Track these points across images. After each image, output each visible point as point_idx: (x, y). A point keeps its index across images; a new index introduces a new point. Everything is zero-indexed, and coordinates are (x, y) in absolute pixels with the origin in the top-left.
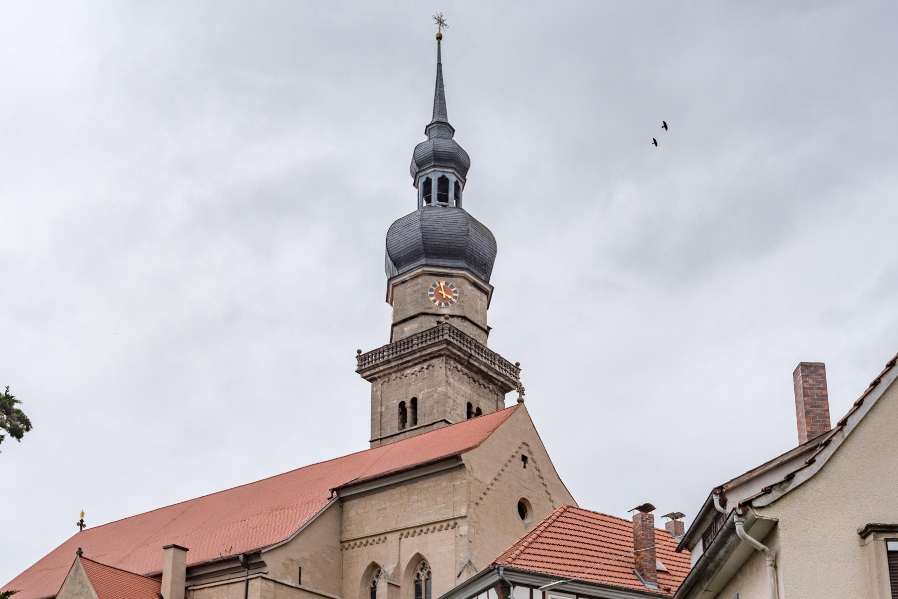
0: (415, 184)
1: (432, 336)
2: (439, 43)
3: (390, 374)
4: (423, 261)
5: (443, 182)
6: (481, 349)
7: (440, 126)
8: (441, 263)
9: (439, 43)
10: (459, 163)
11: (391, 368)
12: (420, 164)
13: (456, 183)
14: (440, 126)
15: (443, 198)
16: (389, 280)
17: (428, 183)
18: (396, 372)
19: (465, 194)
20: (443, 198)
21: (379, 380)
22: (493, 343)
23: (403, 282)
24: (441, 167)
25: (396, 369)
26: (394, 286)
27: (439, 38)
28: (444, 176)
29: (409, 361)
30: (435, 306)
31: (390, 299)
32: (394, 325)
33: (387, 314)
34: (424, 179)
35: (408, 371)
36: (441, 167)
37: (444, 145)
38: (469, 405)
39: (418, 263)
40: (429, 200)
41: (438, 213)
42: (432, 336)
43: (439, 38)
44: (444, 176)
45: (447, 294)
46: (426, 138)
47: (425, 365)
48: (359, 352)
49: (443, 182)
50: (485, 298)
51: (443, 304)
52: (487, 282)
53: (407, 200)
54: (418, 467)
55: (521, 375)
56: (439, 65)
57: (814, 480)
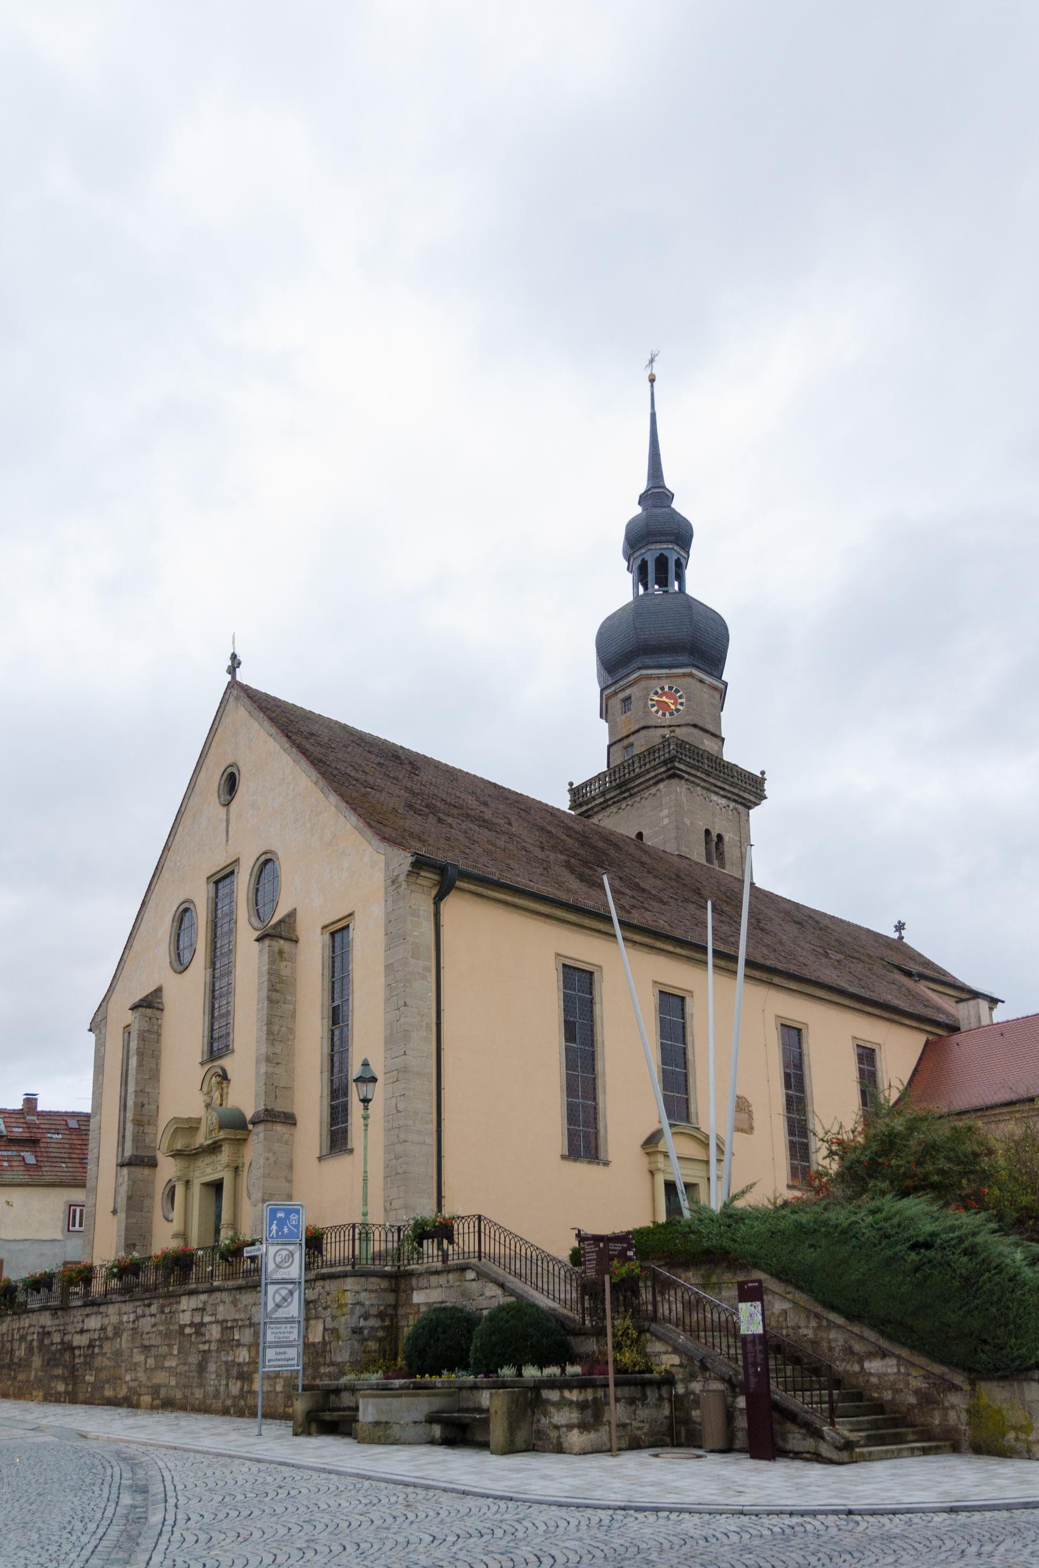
0: (629, 569)
1: (652, 757)
2: (652, 386)
3: (698, 785)
5: (662, 562)
7: (656, 495)
9: (652, 386)
10: (680, 535)
11: (705, 781)
14: (656, 495)
15: (663, 582)
16: (602, 691)
18: (703, 788)
19: (689, 574)
21: (683, 781)
22: (730, 754)
23: (701, 681)
24: (658, 541)
25: (708, 786)
26: (608, 698)
27: (652, 380)
28: (662, 555)
29: (723, 789)
30: (657, 716)
31: (605, 713)
32: (609, 747)
33: (601, 733)
34: (639, 562)
35: (714, 797)
36: (658, 541)
38: (707, 832)
42: (661, 753)
43: (652, 380)
44: (662, 555)
47: (732, 805)
48: (571, 784)
49: (662, 562)
51: (667, 714)
56: (653, 416)
57: (19, 1189)
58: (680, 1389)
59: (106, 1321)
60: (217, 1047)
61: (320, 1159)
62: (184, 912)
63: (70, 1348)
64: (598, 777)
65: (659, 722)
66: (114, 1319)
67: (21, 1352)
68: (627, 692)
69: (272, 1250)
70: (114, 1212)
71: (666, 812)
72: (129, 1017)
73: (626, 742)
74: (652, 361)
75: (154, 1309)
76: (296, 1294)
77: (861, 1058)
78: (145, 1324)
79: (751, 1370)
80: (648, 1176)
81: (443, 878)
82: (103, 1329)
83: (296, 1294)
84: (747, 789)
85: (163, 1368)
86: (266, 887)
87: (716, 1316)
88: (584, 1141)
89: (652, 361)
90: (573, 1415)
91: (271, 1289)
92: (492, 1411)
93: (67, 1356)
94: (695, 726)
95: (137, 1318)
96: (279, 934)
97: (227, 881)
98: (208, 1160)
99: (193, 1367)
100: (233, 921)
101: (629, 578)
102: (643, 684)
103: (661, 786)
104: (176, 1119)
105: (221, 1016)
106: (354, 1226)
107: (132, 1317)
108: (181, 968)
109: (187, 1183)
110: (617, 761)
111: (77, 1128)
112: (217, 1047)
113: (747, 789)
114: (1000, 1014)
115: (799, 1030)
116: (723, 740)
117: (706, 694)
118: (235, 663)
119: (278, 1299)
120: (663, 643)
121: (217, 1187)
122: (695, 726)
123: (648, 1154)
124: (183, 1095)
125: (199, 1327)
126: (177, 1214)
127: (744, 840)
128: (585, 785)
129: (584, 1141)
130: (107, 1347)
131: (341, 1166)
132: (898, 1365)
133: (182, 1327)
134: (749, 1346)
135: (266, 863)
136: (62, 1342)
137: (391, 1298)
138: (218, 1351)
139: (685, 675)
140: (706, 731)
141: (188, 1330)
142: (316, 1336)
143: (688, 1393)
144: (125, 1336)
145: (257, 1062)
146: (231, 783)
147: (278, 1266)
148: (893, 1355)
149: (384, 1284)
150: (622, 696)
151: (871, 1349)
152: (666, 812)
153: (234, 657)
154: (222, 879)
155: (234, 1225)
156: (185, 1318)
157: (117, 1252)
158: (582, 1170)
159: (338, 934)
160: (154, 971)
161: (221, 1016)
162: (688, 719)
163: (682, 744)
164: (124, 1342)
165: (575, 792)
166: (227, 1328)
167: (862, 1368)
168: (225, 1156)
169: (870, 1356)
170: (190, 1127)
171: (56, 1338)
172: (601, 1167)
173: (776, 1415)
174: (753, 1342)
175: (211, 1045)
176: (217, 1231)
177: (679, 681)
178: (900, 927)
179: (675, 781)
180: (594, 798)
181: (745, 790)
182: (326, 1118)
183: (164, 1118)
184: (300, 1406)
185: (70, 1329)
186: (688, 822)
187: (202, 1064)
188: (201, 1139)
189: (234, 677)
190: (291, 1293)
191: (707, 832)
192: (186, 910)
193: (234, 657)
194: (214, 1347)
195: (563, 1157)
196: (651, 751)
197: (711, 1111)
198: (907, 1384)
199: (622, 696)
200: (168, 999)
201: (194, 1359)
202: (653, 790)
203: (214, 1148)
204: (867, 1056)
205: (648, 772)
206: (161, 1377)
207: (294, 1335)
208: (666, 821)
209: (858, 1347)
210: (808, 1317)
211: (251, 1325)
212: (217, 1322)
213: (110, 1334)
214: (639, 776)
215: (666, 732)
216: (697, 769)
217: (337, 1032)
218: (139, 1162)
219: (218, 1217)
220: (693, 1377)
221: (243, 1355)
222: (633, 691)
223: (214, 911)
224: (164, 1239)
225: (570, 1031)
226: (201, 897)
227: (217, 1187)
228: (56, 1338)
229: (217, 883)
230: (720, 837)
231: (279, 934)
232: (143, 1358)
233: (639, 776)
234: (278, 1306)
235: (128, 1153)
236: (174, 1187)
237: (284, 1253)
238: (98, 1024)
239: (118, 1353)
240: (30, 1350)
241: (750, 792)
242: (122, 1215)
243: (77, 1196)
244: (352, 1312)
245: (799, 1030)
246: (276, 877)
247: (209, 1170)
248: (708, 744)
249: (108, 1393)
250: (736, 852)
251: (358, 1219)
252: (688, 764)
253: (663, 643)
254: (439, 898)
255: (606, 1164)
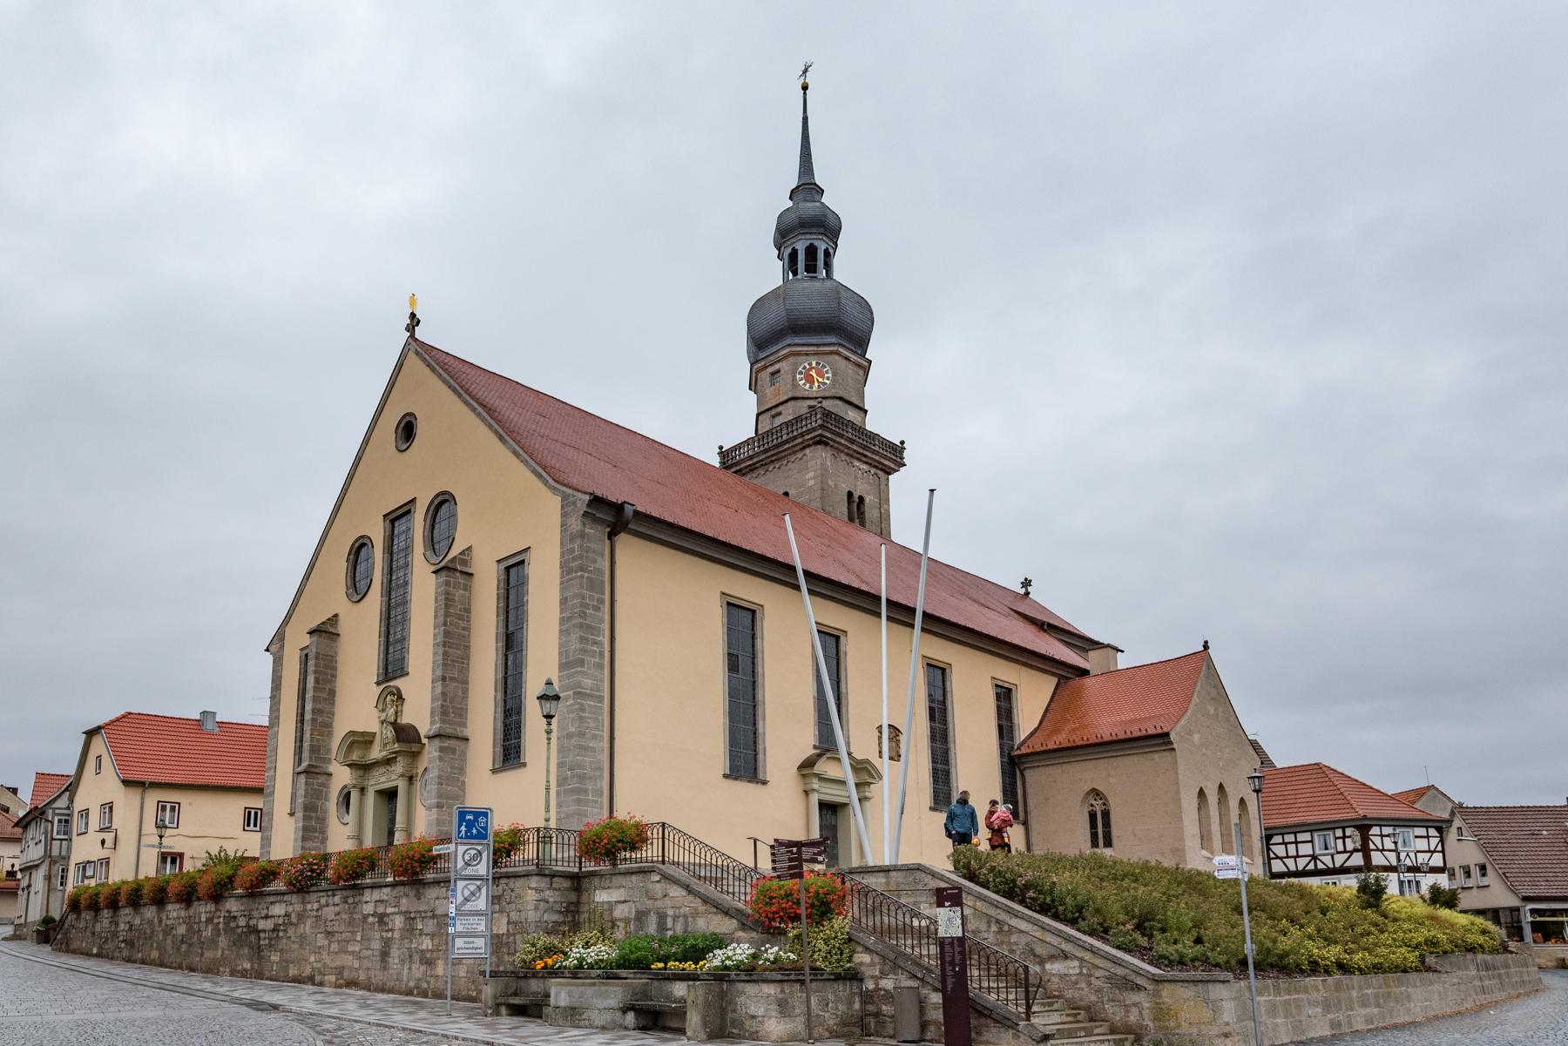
4: (789, 341)
5: (811, 251)
6: (861, 430)
7: (807, 188)
8: (798, 341)
10: (828, 227)
12: (784, 233)
13: (826, 251)
14: (807, 188)
15: (811, 268)
17: (793, 256)
19: (837, 262)
20: (811, 268)
22: (872, 425)
23: (847, 359)
24: (808, 233)
27: (805, 88)
31: (753, 386)
32: (758, 415)
34: (789, 250)
35: (856, 463)
36: (808, 233)
37: (809, 208)
38: (850, 494)
39: (784, 343)
40: (795, 273)
41: (805, 284)
43: (805, 88)
45: (814, 375)
46: (790, 204)
49: (811, 251)
50: (861, 372)
52: (863, 355)
53: (770, 274)
54: (762, 558)
55: (905, 454)
56: (805, 119)
58: (870, 985)
59: (290, 909)
60: (392, 668)
61: (494, 771)
62: (360, 548)
63: (255, 931)
64: (747, 442)
65: (806, 394)
66: (298, 907)
67: (208, 933)
68: (777, 367)
69: (462, 849)
70: (292, 814)
71: (811, 474)
72: (306, 640)
73: (774, 412)
74: (805, 71)
75: (337, 899)
76: (484, 890)
77: (998, 696)
78: (329, 912)
79: (949, 968)
80: (802, 796)
81: (613, 518)
82: (287, 915)
83: (484, 890)
84: (888, 457)
85: (346, 952)
86: (441, 527)
87: (900, 917)
88: (745, 762)
89: (805, 71)
90: (757, 1009)
91: (461, 884)
92: (689, 1001)
93: (253, 938)
94: (841, 399)
95: (321, 907)
96: (455, 572)
97: (404, 520)
98: (382, 770)
99: (377, 953)
100: (408, 549)
101: (778, 266)
102: (791, 359)
103: (807, 451)
104: (352, 733)
105: (397, 642)
106: (538, 830)
107: (316, 906)
108: (357, 598)
109: (363, 790)
110: (765, 426)
111: (257, 740)
112: (392, 668)
113: (888, 457)
114: (1123, 662)
115: (944, 670)
116: (866, 412)
117: (850, 370)
118: (414, 320)
119: (467, 893)
120: (811, 324)
121: (390, 795)
122: (841, 399)
123: (804, 776)
124: (358, 708)
125: (382, 918)
126: (351, 818)
127: (883, 499)
128: (734, 449)
129: (745, 762)
130: (291, 932)
131: (510, 777)
132: (1081, 967)
133: (365, 917)
134: (947, 948)
135: (443, 502)
136: (248, 926)
137: (573, 897)
138: (402, 938)
139: (831, 353)
140: (850, 403)
141: (371, 919)
142: (502, 928)
143: (877, 989)
144: (309, 922)
145: (433, 682)
146: (407, 430)
147: (467, 864)
148: (1077, 958)
149: (566, 884)
150: (771, 369)
151: (1053, 951)
152: (811, 474)
153: (413, 315)
154: (398, 517)
155: (408, 831)
156: (368, 909)
157: (432, 723)
158: (742, 788)
159: (513, 570)
160: (332, 599)
161: (397, 642)
162: (832, 393)
163: (827, 414)
164: (307, 927)
165: (724, 454)
166: (409, 918)
167: (1044, 969)
168: (399, 767)
169: (1052, 958)
170: (362, 740)
171: (242, 922)
172: (760, 786)
173: (973, 1014)
174: (952, 944)
175: (386, 668)
176: (391, 833)
177: (826, 358)
178: (1027, 583)
179: (819, 447)
180: (743, 461)
181: (886, 457)
182: (500, 736)
183: (340, 731)
184: (488, 991)
185: (255, 913)
186: (831, 483)
187: (378, 683)
188: (376, 753)
189: (412, 336)
190: (479, 888)
191: (850, 494)
192: (363, 545)
193: (413, 315)
194: (397, 935)
195: (725, 776)
196: (798, 419)
197: (859, 740)
198: (1089, 984)
199: (771, 369)
200: (343, 627)
201: (376, 945)
202: (799, 455)
203: (388, 761)
204: (1004, 695)
205: (795, 438)
206: (347, 960)
207: (482, 927)
208: (811, 483)
209: (1039, 950)
210: (989, 923)
211: (434, 917)
212: (400, 913)
213: (294, 920)
214: (787, 442)
215: (813, 403)
216: (842, 436)
217: (511, 658)
218: (312, 772)
219: (392, 821)
220: (883, 975)
221: (427, 943)
222: (784, 366)
223: (389, 546)
224: (340, 839)
225: (733, 664)
226: (378, 536)
227: (390, 795)
228: (242, 922)
229: (393, 521)
230: (861, 499)
231: (455, 572)
232: (461, 884)
233: (787, 442)
234: (467, 900)
235: (304, 765)
236: (349, 794)
237: (473, 852)
238: (277, 645)
239: (302, 937)
240: (217, 931)
241: (890, 459)
242: (300, 814)
243: (255, 802)
244: (536, 908)
245: (944, 670)
246: (453, 516)
247: (383, 779)
248: (852, 415)
249: (293, 972)
250: (876, 513)
251: (542, 824)
252: (833, 432)
253: (811, 324)
254: (612, 535)
255: (764, 783)
